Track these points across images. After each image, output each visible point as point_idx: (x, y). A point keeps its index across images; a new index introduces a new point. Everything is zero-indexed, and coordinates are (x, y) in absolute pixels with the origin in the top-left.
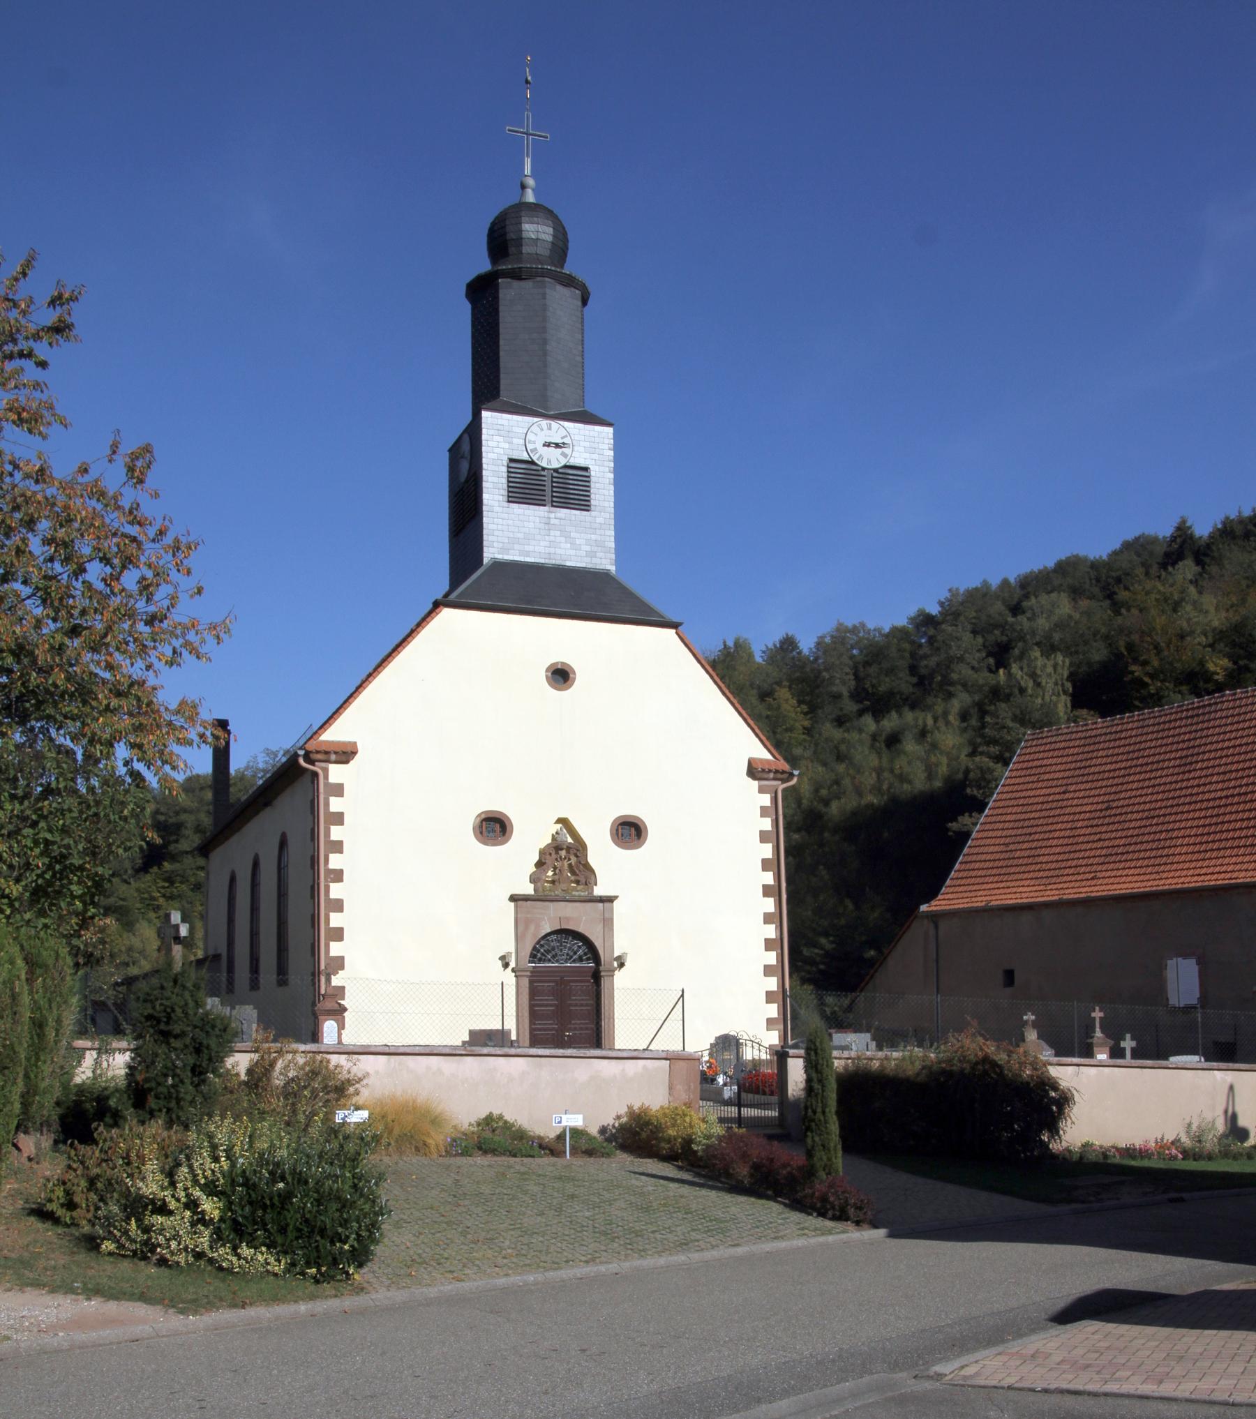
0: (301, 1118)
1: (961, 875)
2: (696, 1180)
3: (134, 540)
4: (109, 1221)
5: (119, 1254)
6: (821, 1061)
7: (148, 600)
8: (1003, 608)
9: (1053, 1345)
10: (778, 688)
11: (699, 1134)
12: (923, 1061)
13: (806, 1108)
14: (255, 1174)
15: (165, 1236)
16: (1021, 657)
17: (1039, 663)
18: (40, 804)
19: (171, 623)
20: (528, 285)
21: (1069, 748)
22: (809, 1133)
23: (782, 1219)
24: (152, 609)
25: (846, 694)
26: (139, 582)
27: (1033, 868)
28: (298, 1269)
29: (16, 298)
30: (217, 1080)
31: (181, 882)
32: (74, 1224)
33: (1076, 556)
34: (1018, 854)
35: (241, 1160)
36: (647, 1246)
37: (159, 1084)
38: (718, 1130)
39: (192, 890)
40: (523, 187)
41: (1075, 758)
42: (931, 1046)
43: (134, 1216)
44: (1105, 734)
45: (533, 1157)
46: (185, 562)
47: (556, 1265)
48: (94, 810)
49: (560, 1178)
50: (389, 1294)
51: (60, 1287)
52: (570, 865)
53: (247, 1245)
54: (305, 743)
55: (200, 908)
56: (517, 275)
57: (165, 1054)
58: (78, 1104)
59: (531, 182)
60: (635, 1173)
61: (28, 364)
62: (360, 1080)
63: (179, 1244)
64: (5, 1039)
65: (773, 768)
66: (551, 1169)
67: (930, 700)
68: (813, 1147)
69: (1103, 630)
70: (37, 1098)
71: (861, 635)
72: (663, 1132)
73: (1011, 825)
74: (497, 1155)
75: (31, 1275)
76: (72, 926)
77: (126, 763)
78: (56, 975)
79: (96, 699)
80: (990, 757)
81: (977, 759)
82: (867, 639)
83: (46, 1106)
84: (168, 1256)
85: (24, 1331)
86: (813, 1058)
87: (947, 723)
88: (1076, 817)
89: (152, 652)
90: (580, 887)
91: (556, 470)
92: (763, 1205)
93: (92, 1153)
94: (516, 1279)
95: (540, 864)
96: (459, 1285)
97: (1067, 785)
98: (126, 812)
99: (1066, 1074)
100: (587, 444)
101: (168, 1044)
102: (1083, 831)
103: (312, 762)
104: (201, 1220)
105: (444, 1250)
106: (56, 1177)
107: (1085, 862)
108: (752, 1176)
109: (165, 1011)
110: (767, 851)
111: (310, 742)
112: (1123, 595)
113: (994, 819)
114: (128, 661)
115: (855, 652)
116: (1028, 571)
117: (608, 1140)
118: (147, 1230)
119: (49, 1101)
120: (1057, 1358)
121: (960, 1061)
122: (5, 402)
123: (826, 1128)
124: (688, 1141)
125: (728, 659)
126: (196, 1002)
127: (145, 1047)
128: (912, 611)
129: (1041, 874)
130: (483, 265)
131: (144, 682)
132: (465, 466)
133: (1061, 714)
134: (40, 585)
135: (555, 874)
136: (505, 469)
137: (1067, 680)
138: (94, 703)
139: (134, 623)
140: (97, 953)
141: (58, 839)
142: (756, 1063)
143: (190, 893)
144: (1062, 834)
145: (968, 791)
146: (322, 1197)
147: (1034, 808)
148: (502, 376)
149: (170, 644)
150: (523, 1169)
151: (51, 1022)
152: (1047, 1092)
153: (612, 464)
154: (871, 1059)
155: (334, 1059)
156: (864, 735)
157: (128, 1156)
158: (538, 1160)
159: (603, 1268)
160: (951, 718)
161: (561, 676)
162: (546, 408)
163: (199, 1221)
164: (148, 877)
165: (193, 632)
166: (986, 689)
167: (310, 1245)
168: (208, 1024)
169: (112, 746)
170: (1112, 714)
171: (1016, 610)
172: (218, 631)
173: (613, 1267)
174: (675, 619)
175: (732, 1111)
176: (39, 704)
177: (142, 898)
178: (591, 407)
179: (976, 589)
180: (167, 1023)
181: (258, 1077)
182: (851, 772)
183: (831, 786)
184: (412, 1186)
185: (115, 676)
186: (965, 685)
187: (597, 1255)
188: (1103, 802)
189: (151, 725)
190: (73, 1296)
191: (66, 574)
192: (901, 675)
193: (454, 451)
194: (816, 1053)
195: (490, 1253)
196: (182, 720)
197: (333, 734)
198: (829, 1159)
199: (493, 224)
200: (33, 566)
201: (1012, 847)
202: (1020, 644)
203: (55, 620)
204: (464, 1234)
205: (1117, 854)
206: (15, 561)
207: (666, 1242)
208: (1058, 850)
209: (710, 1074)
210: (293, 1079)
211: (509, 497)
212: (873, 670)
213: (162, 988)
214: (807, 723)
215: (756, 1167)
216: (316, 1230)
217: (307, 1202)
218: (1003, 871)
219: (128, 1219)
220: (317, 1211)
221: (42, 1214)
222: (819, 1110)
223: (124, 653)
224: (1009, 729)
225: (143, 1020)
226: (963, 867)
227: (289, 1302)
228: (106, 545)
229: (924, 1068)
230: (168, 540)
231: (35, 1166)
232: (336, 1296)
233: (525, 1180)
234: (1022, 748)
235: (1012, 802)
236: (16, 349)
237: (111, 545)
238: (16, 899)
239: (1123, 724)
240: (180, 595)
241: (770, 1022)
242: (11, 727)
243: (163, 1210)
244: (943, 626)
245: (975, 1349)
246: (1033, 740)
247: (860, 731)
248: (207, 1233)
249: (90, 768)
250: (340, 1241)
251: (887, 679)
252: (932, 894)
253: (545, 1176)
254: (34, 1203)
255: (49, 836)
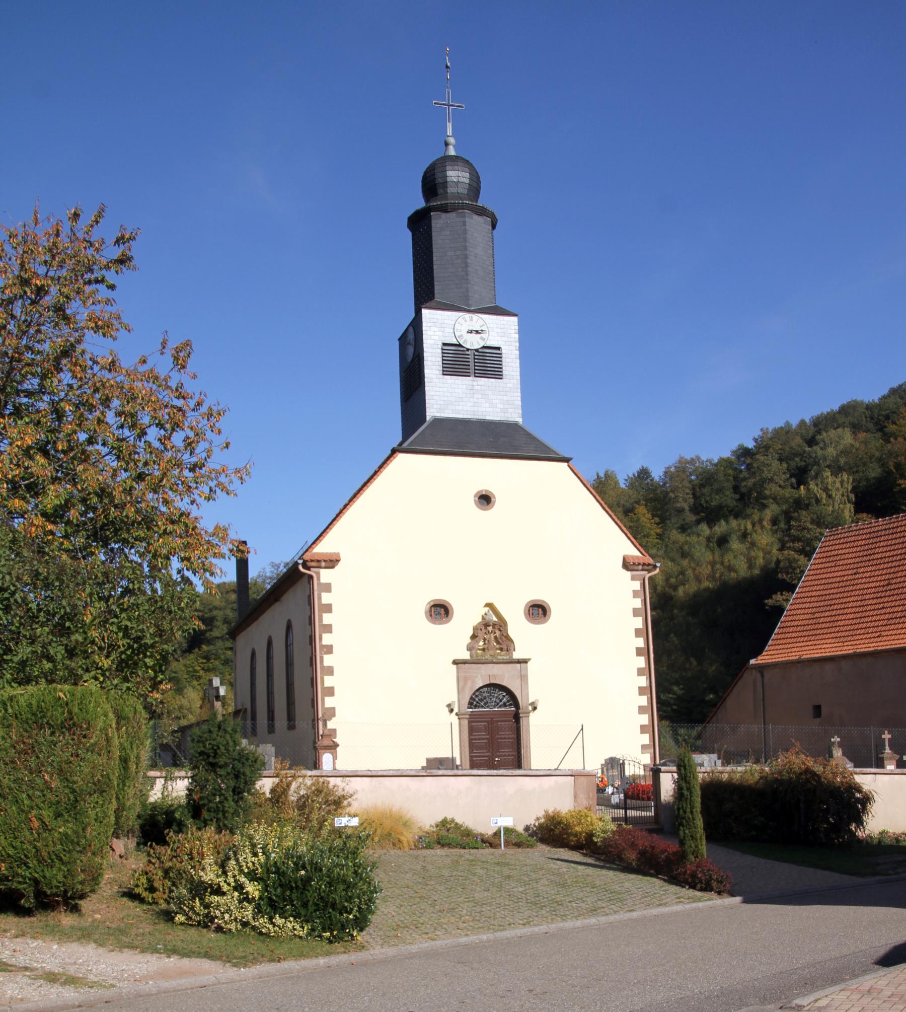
0: (315, 823)
1: (779, 636)
2: (597, 863)
3: (180, 409)
4: (180, 902)
5: (188, 924)
6: (689, 774)
7: (192, 453)
8: (801, 441)
9: (882, 983)
10: (637, 506)
11: (598, 829)
12: (761, 773)
13: (679, 809)
14: (284, 865)
15: (220, 911)
16: (816, 477)
17: (830, 480)
18: (122, 601)
19: (208, 470)
20: (452, 215)
21: (858, 541)
22: (681, 828)
23: (663, 891)
24: (194, 459)
25: (687, 508)
26: (184, 440)
27: (833, 630)
28: (316, 934)
29: (92, 240)
30: (250, 797)
31: (215, 659)
32: (155, 903)
33: (855, 401)
34: (822, 620)
35: (273, 855)
36: (567, 912)
37: (210, 801)
38: (612, 827)
39: (223, 664)
40: (447, 144)
41: (863, 548)
42: (766, 762)
43: (198, 896)
44: (885, 530)
45: (477, 848)
46: (217, 424)
47: (502, 928)
48: (159, 604)
49: (498, 864)
50: (383, 951)
51: (147, 948)
52: (496, 637)
53: (280, 916)
54: (303, 555)
55: (229, 677)
56: (444, 209)
57: (214, 780)
58: (152, 816)
59: (452, 140)
60: (552, 859)
61: (102, 287)
62: (351, 796)
63: (231, 916)
64: (103, 771)
65: (641, 562)
66: (491, 857)
67: (749, 511)
68: (684, 837)
69: (877, 454)
70: (125, 813)
71: (697, 465)
72: (572, 829)
73: (816, 599)
74: (451, 848)
75: (127, 940)
76: (147, 688)
77: (179, 572)
78: (135, 724)
79: (157, 525)
80: (795, 551)
81: (786, 552)
82: (702, 468)
83: (132, 819)
84: (223, 925)
85: (124, 980)
86: (683, 772)
87: (762, 527)
88: (865, 592)
89: (195, 491)
90: (503, 653)
91: (477, 350)
92: (648, 881)
93: (165, 852)
94: (474, 938)
95: (474, 637)
96: (433, 943)
97: (857, 568)
98: (182, 604)
99: (866, 780)
100: (499, 330)
101: (215, 772)
102: (870, 602)
103: (309, 568)
104: (246, 898)
105: (419, 917)
106: (140, 869)
107: (872, 624)
108: (638, 860)
109: (212, 748)
110: (639, 622)
111: (307, 554)
112: (892, 428)
113: (803, 595)
114: (178, 497)
115: (693, 477)
116: (819, 414)
117: (531, 835)
118: (207, 906)
119: (133, 815)
120: (887, 992)
121: (788, 772)
122: (86, 314)
123: (694, 823)
124: (590, 835)
125: (601, 486)
126: (234, 742)
127: (199, 775)
128: (734, 447)
129: (839, 634)
130: (421, 204)
131: (189, 514)
132: (411, 350)
133: (847, 518)
134: (115, 445)
135: (485, 644)
136: (440, 351)
137: (851, 492)
138: (156, 529)
139: (182, 470)
140: (159, 711)
141: (135, 626)
142: (634, 777)
143: (221, 667)
144: (855, 604)
145: (780, 576)
146: (333, 880)
147: (833, 586)
148: (436, 283)
149: (207, 484)
150: (471, 858)
151: (133, 759)
152: (854, 794)
153: (517, 344)
154: (722, 773)
155: (333, 781)
156: (701, 538)
157: (191, 854)
158: (481, 851)
159: (536, 929)
160: (765, 523)
161: (485, 499)
162: (468, 305)
163: (244, 899)
164: (192, 656)
165: (223, 475)
166: (791, 500)
167: (325, 916)
168: (243, 757)
169: (169, 559)
170: (883, 516)
171: (811, 442)
172: (241, 474)
173: (544, 928)
174: (567, 456)
175: (621, 813)
176: (116, 531)
177: (188, 671)
178: (500, 303)
179: (781, 428)
180: (215, 757)
181: (279, 795)
182: (693, 565)
183: (678, 575)
184: (392, 871)
185: (170, 509)
186: (775, 499)
187: (531, 919)
188: (884, 580)
189: (196, 543)
190: (158, 955)
191: (132, 437)
192: (728, 493)
193: (403, 340)
194: (685, 769)
195: (453, 919)
196: (217, 540)
197: (321, 548)
198: (696, 846)
199: (426, 173)
200: (109, 432)
201: (816, 615)
202: (815, 467)
203: (126, 470)
204: (433, 905)
205: (896, 618)
206: (97, 428)
207: (580, 909)
208: (852, 616)
209: (601, 785)
210: (303, 796)
211: (443, 371)
212: (706, 490)
213: (210, 732)
214: (658, 531)
215: (642, 853)
216: (329, 904)
217: (322, 884)
218: (811, 633)
219: (194, 898)
220: (330, 891)
221: (131, 895)
222: (688, 810)
223: (175, 491)
224: (809, 530)
225: (197, 755)
226: (781, 631)
227: (311, 957)
228: (161, 414)
229: (761, 778)
230: (204, 409)
231: (125, 862)
232: (345, 952)
233: (474, 865)
234: (823, 542)
235: (816, 582)
236: (93, 277)
237: (164, 415)
238: (106, 670)
239: (898, 522)
240: (213, 449)
241: (644, 747)
242: (98, 548)
243: (218, 892)
244: (757, 456)
245: (823, 987)
246: (831, 536)
247: (698, 535)
248: (250, 908)
249: (156, 573)
250: (347, 912)
251: (717, 497)
252: (757, 652)
253: (487, 862)
254: (125, 888)
255: (128, 624)
